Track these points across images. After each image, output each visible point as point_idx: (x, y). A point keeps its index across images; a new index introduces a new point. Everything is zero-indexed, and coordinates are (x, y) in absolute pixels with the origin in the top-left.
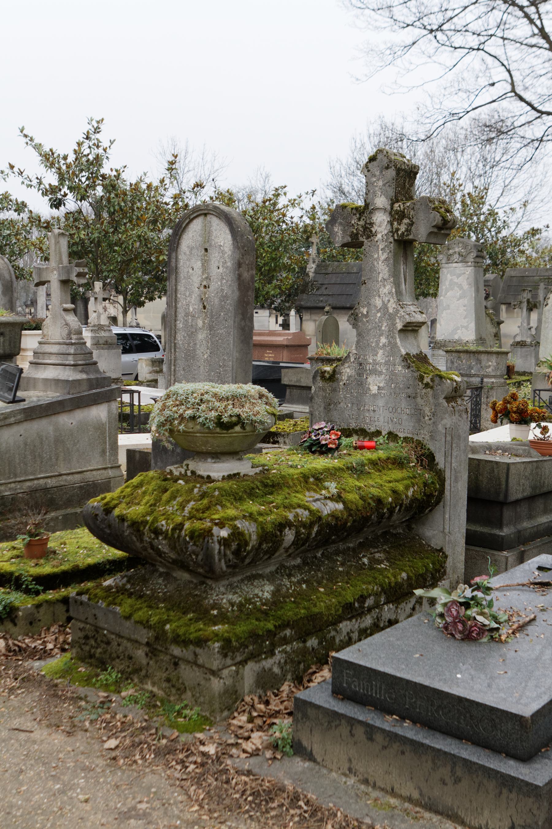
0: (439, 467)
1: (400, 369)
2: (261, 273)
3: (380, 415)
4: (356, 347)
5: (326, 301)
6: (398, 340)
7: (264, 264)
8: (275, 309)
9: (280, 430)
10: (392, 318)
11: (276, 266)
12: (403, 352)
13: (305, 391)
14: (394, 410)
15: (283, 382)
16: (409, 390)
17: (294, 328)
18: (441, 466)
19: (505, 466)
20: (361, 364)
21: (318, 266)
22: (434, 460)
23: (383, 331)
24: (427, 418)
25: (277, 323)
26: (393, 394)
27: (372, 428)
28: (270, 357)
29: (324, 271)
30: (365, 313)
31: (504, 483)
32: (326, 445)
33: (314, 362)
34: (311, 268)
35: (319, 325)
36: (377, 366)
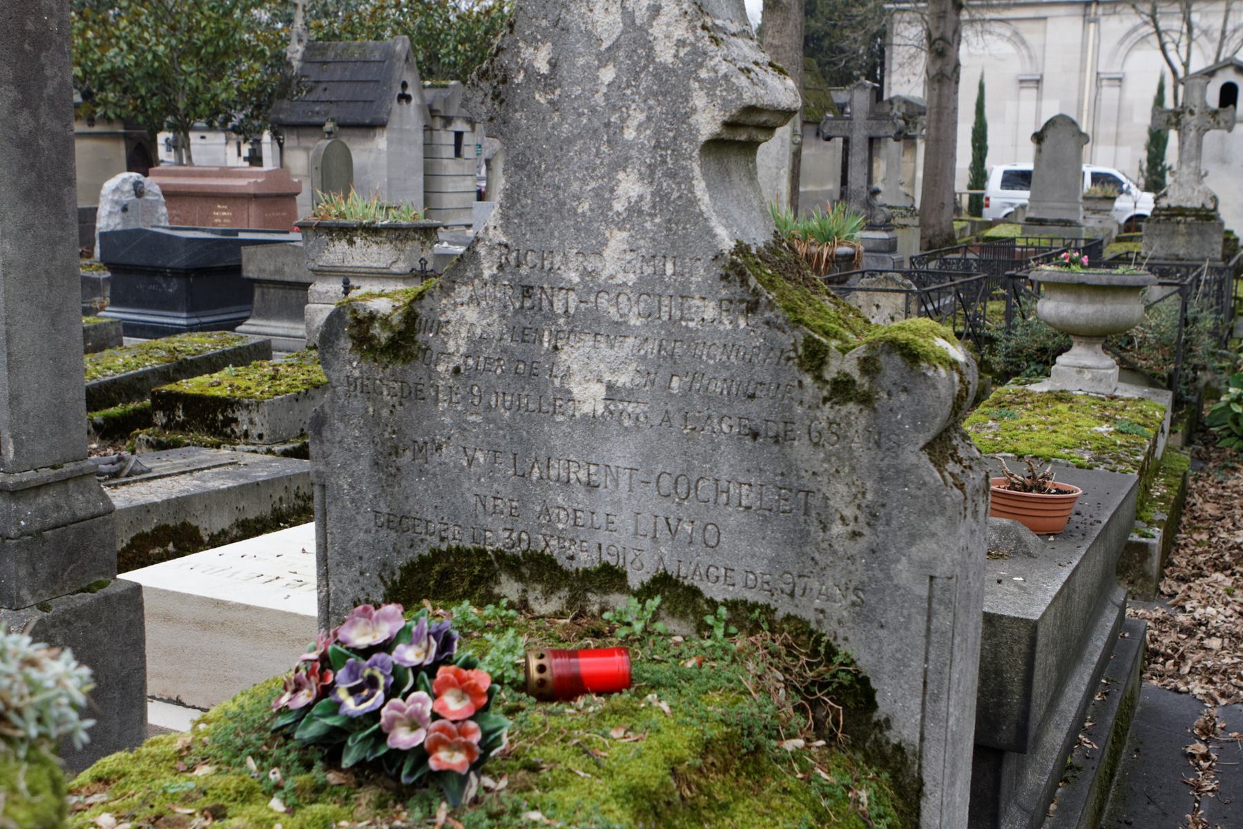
0: (893, 737)
1: (710, 312)
2: (201, 60)
3: (617, 503)
4: (505, 217)
5: (327, 113)
6: (700, 187)
7: (205, 43)
8: (234, 129)
9: (238, 394)
10: (670, 88)
11: (227, 47)
12: (727, 243)
13: (293, 293)
14: (684, 486)
15: (245, 274)
16: (753, 406)
17: (269, 163)
18: (905, 730)
19: (1024, 632)
20: (527, 291)
21: (307, 48)
22: (872, 705)
23: (630, 145)
24: (837, 529)
25: (239, 155)
26: (677, 421)
27: (583, 556)
28: (223, 217)
29: (319, 58)
30: (544, 68)
31: (1016, 688)
32: (421, 754)
33: (310, 233)
34: (295, 52)
35: (315, 158)
36: (603, 301)
